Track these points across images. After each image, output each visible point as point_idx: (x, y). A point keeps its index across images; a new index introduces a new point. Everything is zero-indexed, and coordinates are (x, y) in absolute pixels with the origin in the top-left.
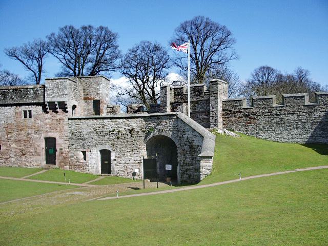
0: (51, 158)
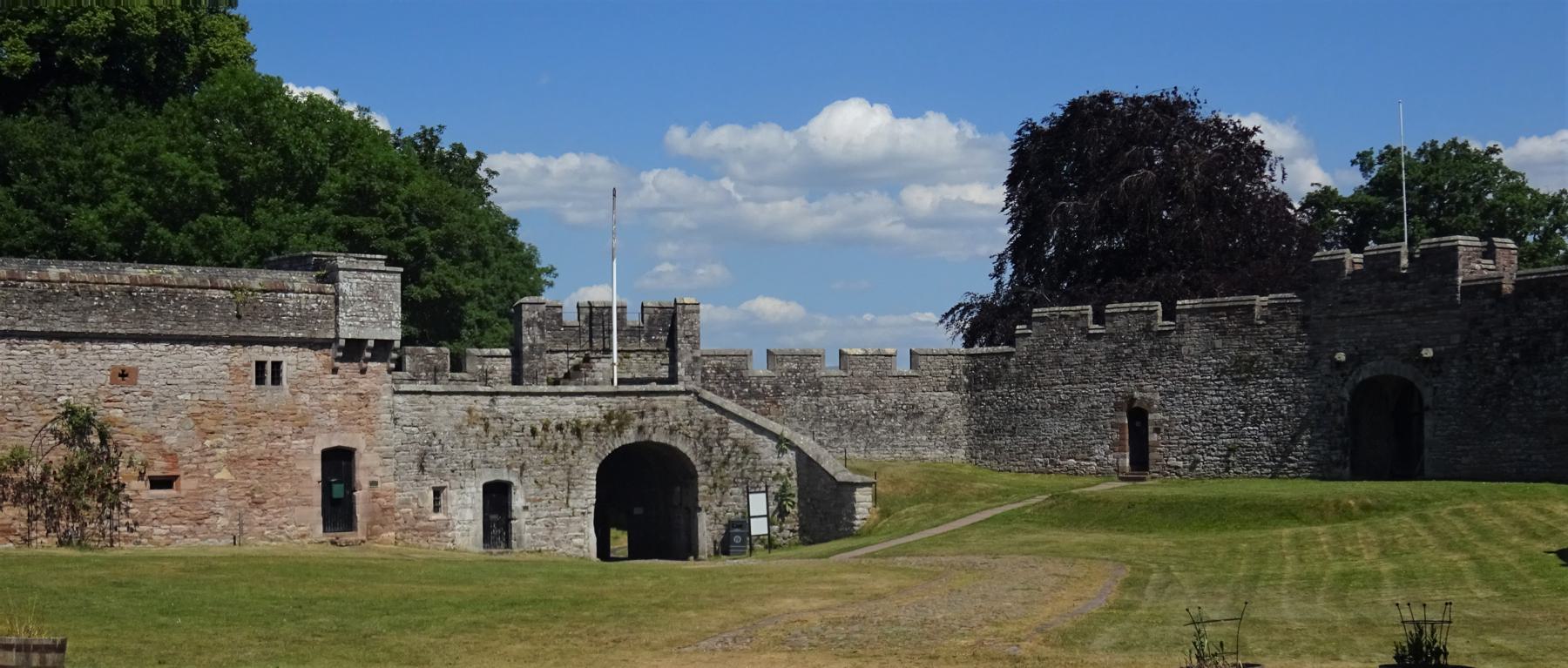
0: (338, 512)
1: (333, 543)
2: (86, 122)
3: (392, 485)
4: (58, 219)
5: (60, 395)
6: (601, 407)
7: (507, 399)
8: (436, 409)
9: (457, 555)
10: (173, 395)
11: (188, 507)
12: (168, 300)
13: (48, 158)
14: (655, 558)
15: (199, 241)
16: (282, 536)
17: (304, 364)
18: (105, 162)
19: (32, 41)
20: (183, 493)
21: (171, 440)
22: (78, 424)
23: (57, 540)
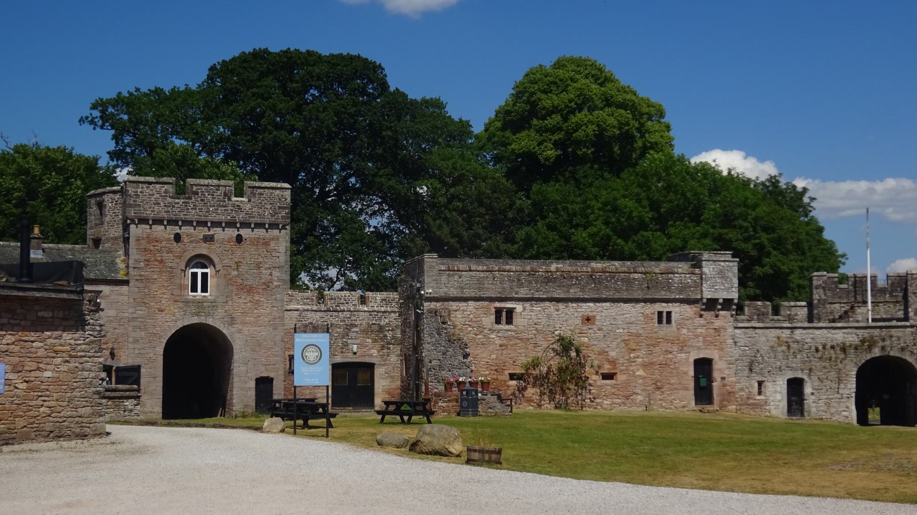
0: (703, 394)
1: (701, 411)
2: (584, 184)
3: (734, 379)
4: (568, 237)
5: (556, 330)
6: (858, 335)
7: (801, 331)
8: (759, 337)
9: (770, 420)
10: (613, 330)
11: (622, 390)
12: (611, 280)
13: (563, 205)
14: (893, 425)
15: (639, 246)
16: (672, 407)
17: (684, 313)
18: (592, 205)
19: (556, 144)
20: (619, 383)
21: (613, 354)
22: (565, 345)
23: (554, 405)
